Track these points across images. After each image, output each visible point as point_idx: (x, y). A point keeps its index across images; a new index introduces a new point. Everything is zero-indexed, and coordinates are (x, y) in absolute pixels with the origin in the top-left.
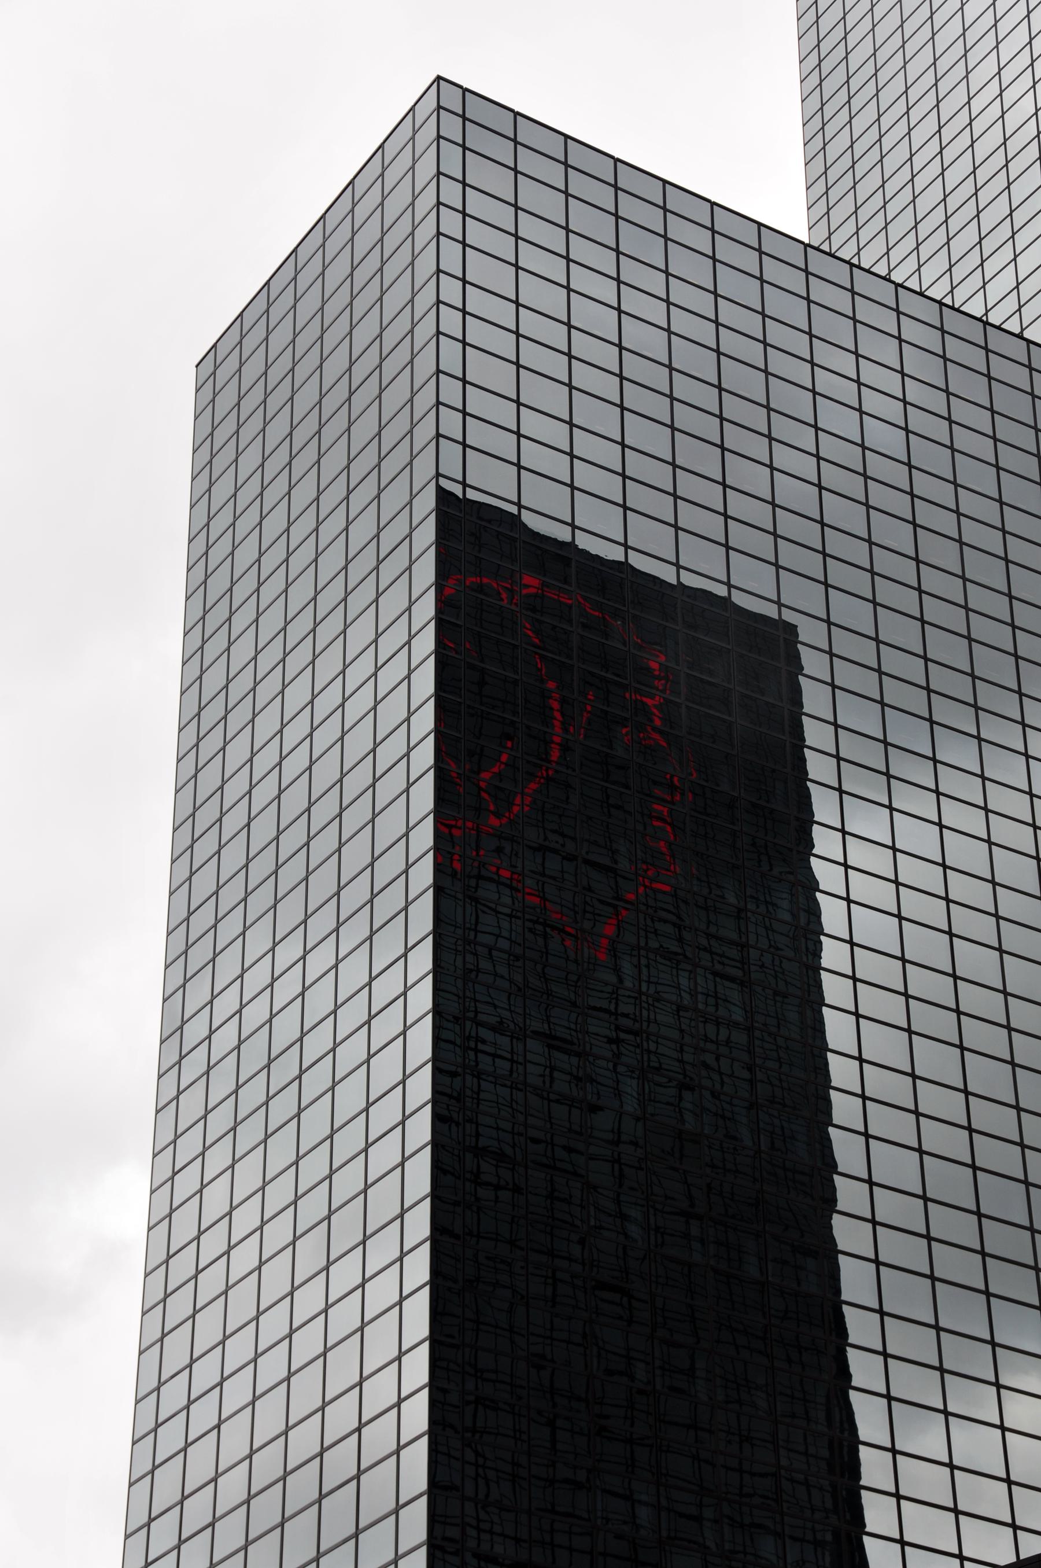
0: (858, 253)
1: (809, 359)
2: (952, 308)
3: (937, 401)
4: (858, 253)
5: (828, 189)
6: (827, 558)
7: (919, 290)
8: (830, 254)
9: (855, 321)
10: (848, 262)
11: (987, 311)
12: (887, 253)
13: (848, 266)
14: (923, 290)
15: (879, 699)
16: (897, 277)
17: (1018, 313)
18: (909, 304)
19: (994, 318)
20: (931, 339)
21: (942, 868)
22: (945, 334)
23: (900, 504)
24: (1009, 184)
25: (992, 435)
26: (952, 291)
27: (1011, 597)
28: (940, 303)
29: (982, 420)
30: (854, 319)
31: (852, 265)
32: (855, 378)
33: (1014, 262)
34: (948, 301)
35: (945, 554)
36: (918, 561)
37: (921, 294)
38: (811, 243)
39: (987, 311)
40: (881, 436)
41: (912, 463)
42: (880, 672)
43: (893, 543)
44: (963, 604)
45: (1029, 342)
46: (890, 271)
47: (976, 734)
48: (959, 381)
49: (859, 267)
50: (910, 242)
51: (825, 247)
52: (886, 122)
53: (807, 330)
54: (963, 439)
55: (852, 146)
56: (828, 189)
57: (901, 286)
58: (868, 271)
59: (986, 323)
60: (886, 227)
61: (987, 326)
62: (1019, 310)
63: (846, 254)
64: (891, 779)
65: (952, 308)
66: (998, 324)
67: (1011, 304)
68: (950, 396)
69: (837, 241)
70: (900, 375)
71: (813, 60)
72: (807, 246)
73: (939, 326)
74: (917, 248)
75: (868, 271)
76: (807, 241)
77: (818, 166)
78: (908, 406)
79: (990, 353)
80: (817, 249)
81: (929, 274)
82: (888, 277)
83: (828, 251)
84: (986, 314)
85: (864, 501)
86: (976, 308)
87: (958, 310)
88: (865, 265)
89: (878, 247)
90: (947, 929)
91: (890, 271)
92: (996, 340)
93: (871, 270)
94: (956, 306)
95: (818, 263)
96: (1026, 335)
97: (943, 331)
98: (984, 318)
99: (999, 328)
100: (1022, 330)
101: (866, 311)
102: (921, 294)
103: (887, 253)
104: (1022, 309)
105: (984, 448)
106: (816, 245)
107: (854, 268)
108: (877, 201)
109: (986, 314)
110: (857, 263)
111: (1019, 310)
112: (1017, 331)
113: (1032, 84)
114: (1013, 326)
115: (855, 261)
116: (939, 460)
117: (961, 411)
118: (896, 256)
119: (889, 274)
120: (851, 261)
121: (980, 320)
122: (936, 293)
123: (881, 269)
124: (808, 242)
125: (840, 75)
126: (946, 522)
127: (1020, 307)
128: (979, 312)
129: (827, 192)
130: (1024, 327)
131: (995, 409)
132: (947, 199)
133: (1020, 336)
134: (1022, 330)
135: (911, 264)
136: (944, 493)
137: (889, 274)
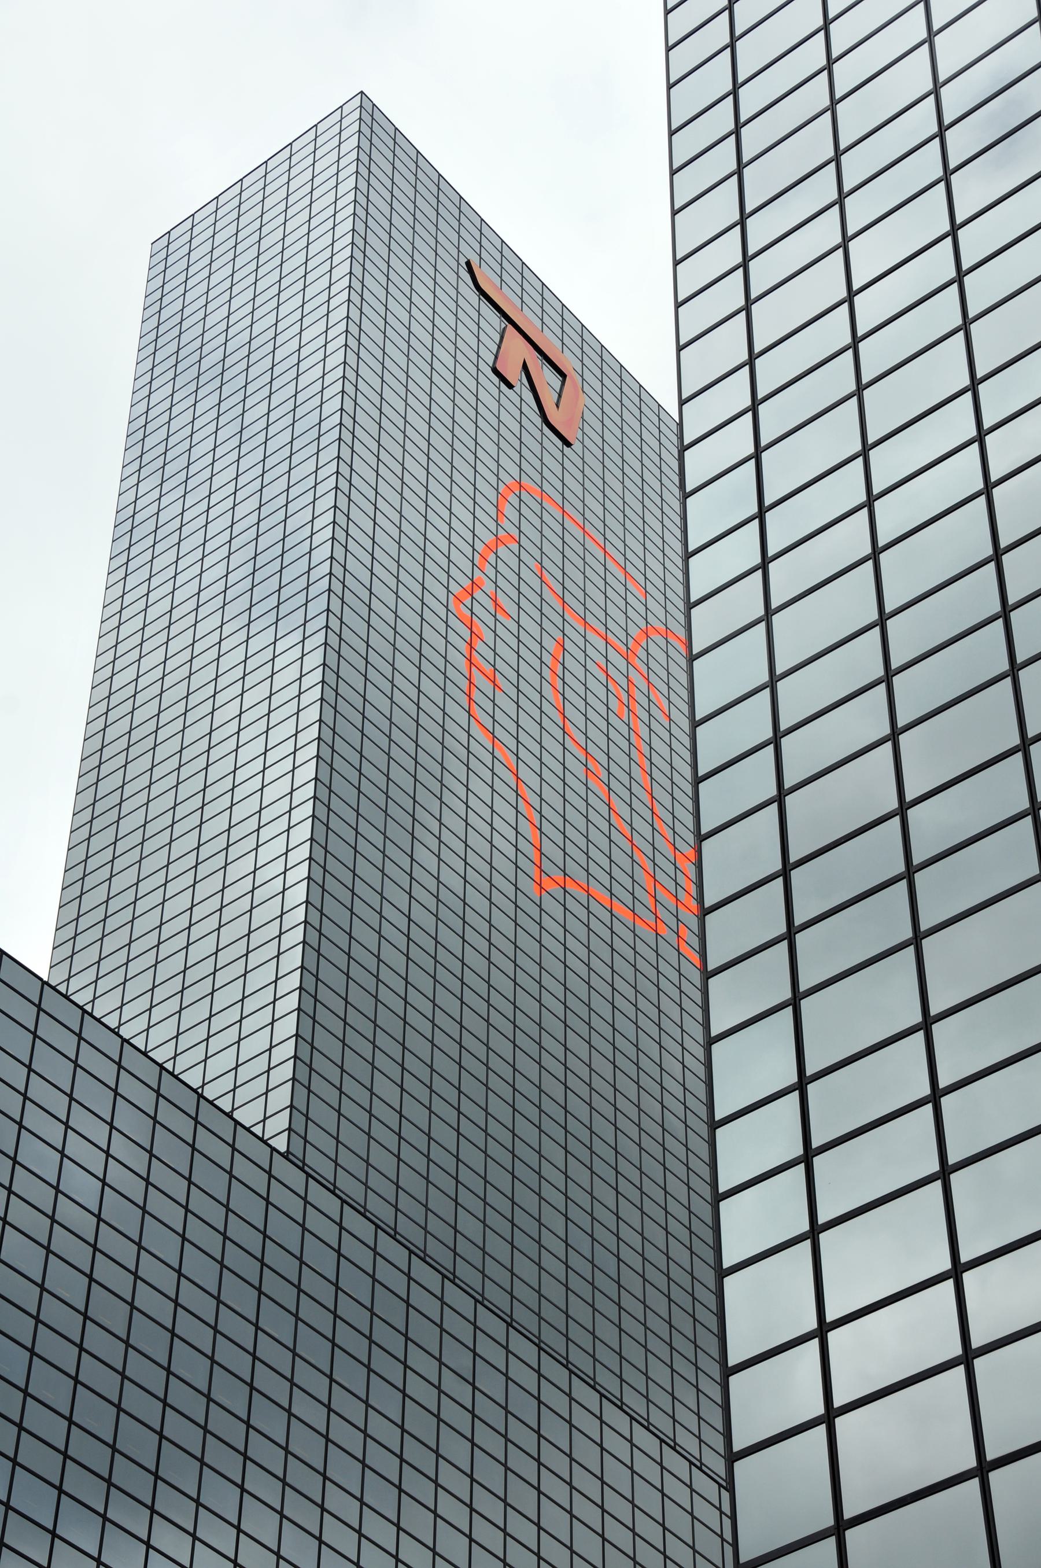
0: (93, 1001)
1: (23, 1091)
2: (172, 1074)
3: (139, 1161)
4: (93, 1001)
5: (86, 861)
6: (32, 1073)
7: (143, 1050)
8: (66, 997)
9: (76, 1065)
10: (81, 1008)
11: (204, 1084)
12: (127, 964)
13: (81, 1011)
14: (148, 1050)
15: (55, 1185)
16: (126, 1032)
17: (239, 1023)
18: (131, 1060)
19: (209, 1093)
20: (146, 1099)
21: (73, 1382)
22: (153, 1158)
23: (81, 1255)
24: (274, 657)
25: (174, 1298)
26: (177, 1037)
27: (169, 1372)
28: (161, 1066)
29: (178, 1188)
30: (75, 1063)
31: (85, 1011)
32: (65, 1120)
33: (237, 1044)
34: (169, 1066)
35: (114, 1316)
36: (86, 1317)
37: (145, 1054)
38: (50, 982)
39: (204, 1084)
40: (77, 1183)
41: (102, 1216)
42: (37, 1320)
43: (64, 1293)
44: (116, 1402)
45: (237, 1123)
46: (120, 1025)
47: (102, 1512)
48: (164, 1144)
49: (91, 1015)
50: (144, 1003)
51: (62, 988)
52: (144, 888)
53: (23, 1091)
54: (156, 1203)
55: (125, 766)
56: (76, 935)
57: (127, 1041)
58: (98, 1020)
59: (201, 1096)
60: (132, 921)
61: (201, 1099)
62: (245, 975)
63: (80, 999)
64: (50, 1254)
65: (172, 1074)
66: (211, 1099)
67: (227, 1083)
68: (146, 1215)
69: (75, 984)
70: (104, 1155)
71: (86, 815)
72: (45, 983)
73: (145, 1177)
74: (150, 1009)
75: (98, 1020)
76: (45, 979)
77: (72, 911)
78: (101, 1223)
79: (189, 1213)
80: (54, 988)
81: (158, 1035)
82: (116, 1030)
83: (65, 993)
84: (202, 1087)
85: (51, 1214)
86: (193, 1079)
87: (176, 1077)
88: (97, 1014)
89: (113, 1001)
90: (63, 1495)
91: (120, 1025)
92: (207, 1115)
93: (102, 1020)
94: (176, 1073)
95: (50, 1002)
96: (236, 1115)
97: (148, 1183)
98: (200, 1091)
99: (211, 1103)
100: (233, 1110)
101: (88, 1058)
102: (145, 1054)
103: (137, 884)
104: (262, 769)
105: (174, 1216)
106: (54, 984)
107: (86, 1015)
108: (121, 957)
109: (202, 1087)
110: (90, 1011)
111: (234, 1090)
112: (228, 1109)
113: (317, 436)
114: (225, 1104)
115: (88, 1008)
116: (128, 1219)
117: (160, 1175)
118: (128, 1012)
119: (118, 1027)
120: (84, 1007)
121: (195, 1091)
122: (159, 1056)
123: (112, 1021)
124: (47, 980)
125: (109, 836)
126: (122, 1283)
127: (235, 1088)
128: (195, 1083)
129: (89, 839)
130: (242, 1037)
131: (186, 1236)
132: (194, 908)
133: (229, 1115)
134: (233, 1110)
135: (141, 1023)
136: (127, 1253)
137: (118, 1027)
